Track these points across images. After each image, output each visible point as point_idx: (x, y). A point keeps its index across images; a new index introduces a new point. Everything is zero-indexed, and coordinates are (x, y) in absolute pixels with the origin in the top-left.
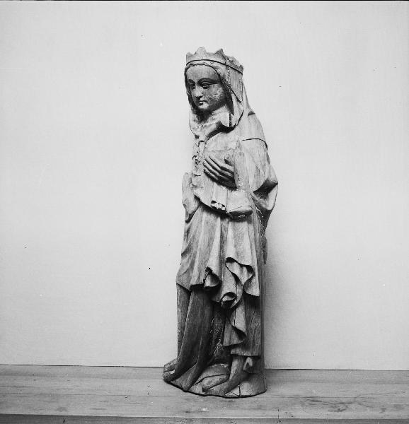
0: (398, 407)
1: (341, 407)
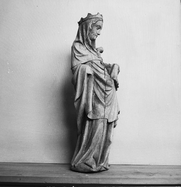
0: (177, 175)
1: (151, 175)
